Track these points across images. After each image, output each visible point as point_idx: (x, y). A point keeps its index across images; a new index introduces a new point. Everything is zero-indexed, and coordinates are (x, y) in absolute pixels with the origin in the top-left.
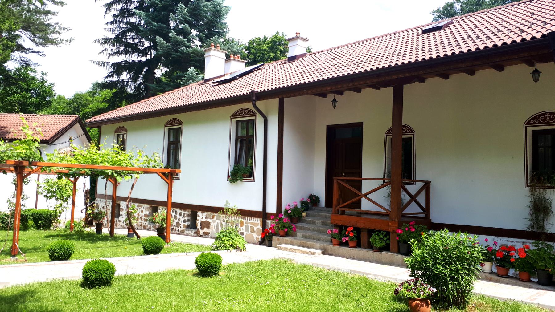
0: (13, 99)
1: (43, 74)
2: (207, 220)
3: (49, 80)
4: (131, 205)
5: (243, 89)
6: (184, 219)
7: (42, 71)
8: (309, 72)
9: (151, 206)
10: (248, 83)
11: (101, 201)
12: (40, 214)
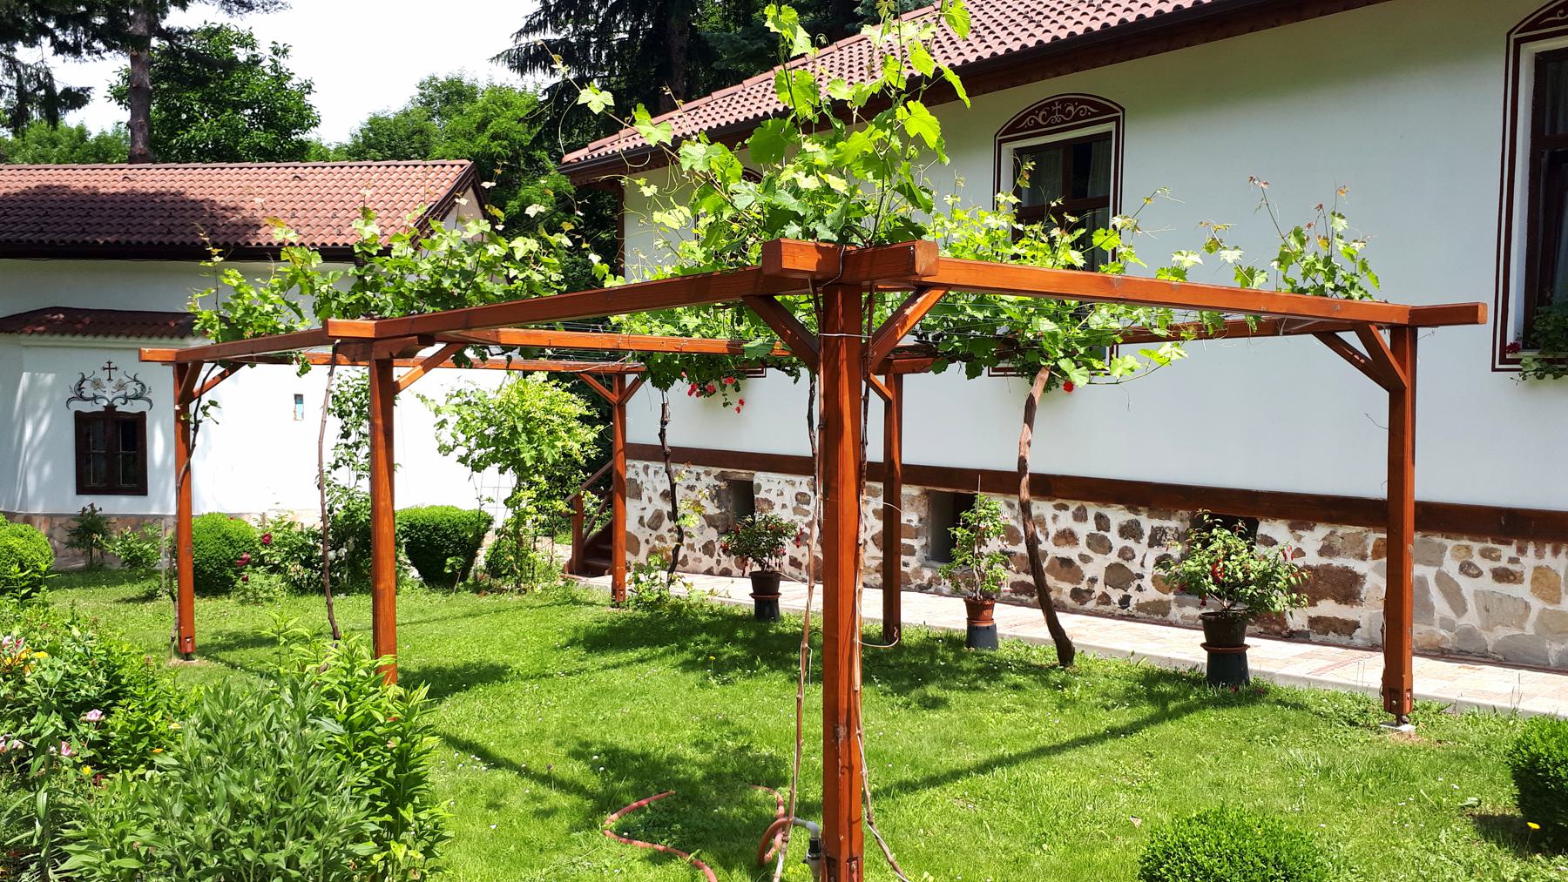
0: (194, 137)
1: (276, 53)
2: (1337, 562)
3: (298, 68)
4: (1052, 516)
5: (754, 101)
6: (1157, 552)
7: (274, 43)
8: (1000, 24)
9: (927, 493)
10: (749, 94)
11: (651, 471)
12: (436, 529)
